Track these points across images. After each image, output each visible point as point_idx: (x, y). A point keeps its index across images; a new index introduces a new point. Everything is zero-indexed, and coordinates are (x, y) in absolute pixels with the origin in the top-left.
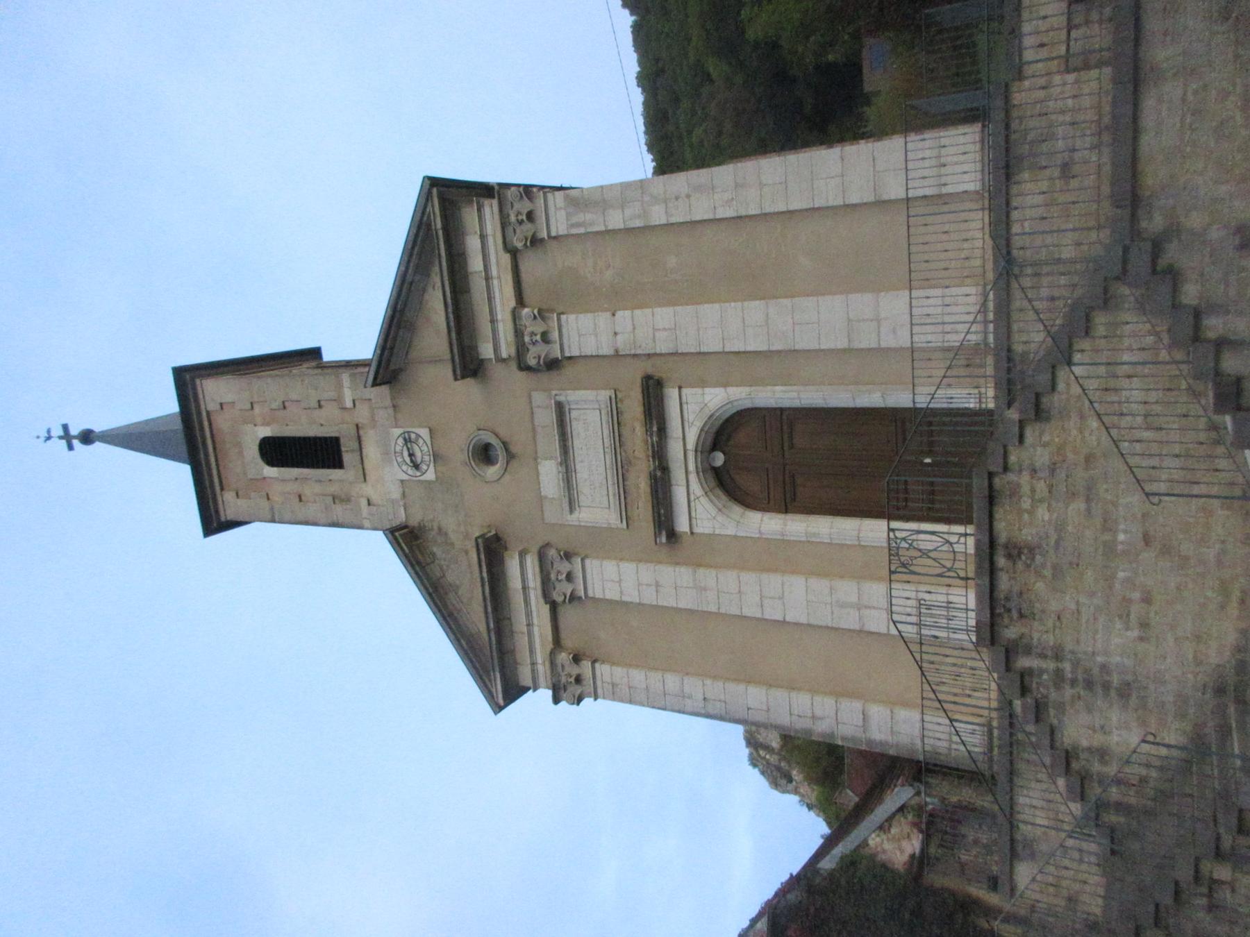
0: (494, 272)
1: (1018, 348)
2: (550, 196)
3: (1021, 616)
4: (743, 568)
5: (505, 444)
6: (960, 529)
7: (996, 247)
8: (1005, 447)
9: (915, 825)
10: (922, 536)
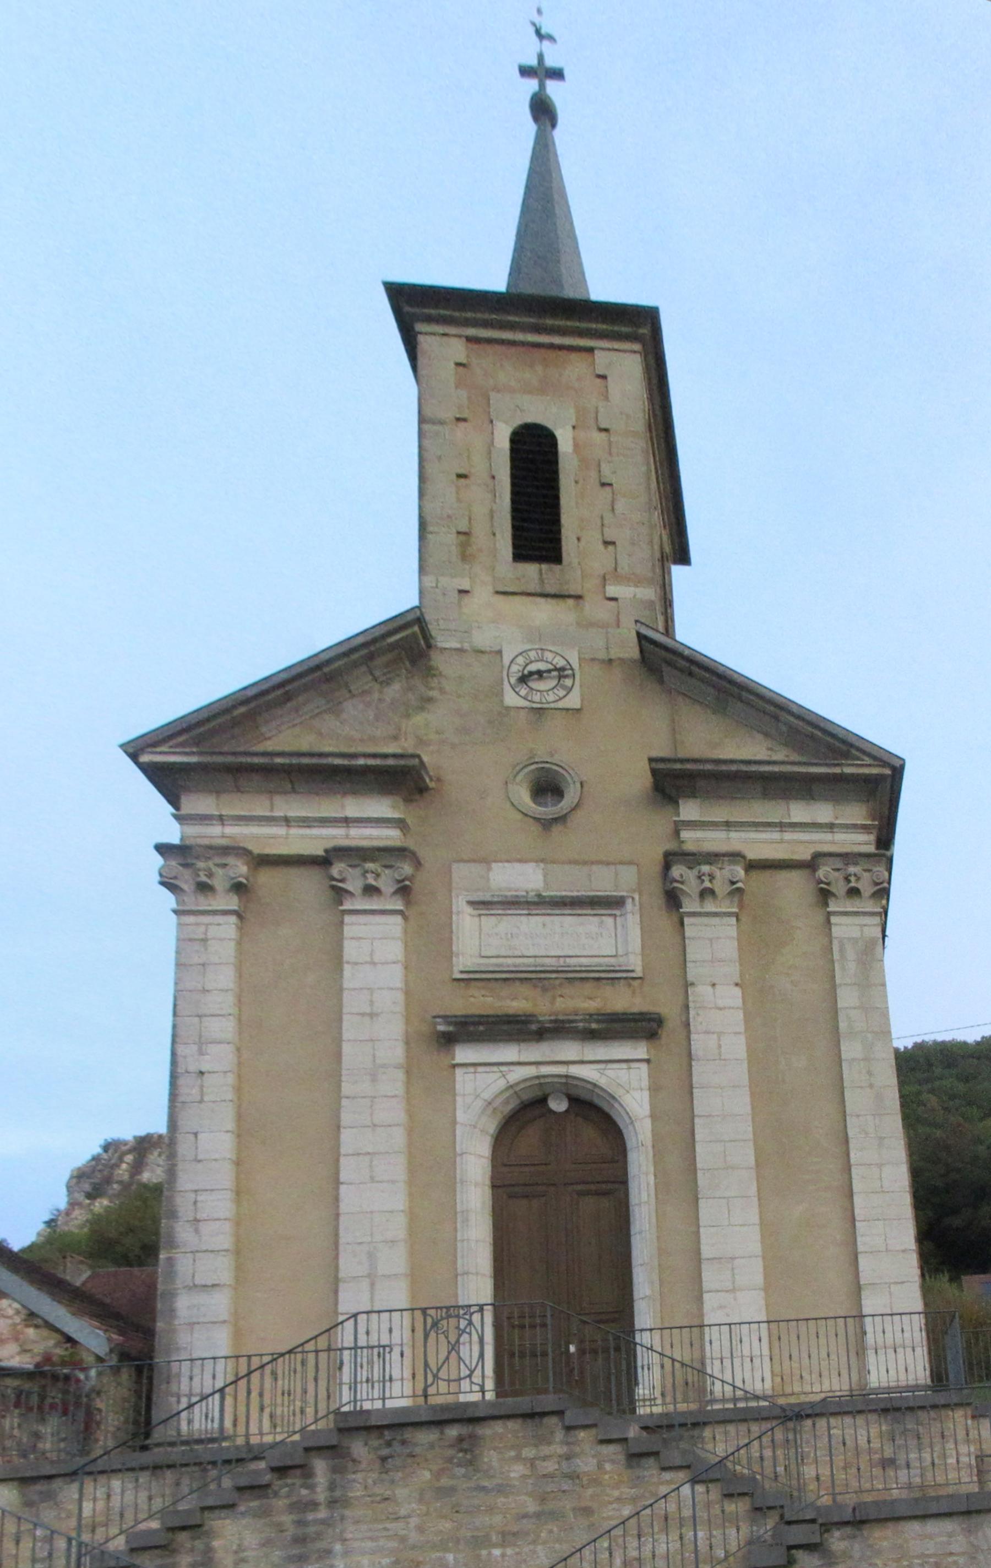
0: (788, 836)
1: (707, 1433)
2: (877, 920)
3: (384, 1459)
4: (410, 1132)
5: (561, 819)
6: (490, 1385)
7: (812, 1405)
8: (595, 1425)
9: (47, 1359)
10: (476, 1348)
